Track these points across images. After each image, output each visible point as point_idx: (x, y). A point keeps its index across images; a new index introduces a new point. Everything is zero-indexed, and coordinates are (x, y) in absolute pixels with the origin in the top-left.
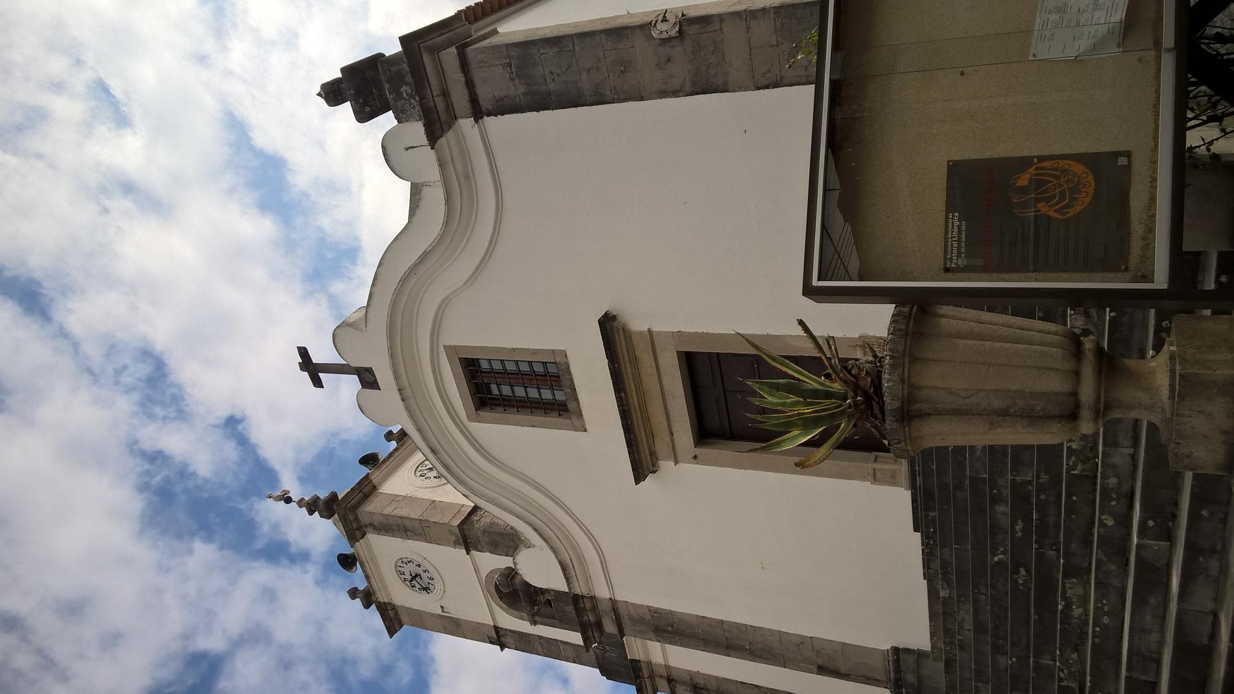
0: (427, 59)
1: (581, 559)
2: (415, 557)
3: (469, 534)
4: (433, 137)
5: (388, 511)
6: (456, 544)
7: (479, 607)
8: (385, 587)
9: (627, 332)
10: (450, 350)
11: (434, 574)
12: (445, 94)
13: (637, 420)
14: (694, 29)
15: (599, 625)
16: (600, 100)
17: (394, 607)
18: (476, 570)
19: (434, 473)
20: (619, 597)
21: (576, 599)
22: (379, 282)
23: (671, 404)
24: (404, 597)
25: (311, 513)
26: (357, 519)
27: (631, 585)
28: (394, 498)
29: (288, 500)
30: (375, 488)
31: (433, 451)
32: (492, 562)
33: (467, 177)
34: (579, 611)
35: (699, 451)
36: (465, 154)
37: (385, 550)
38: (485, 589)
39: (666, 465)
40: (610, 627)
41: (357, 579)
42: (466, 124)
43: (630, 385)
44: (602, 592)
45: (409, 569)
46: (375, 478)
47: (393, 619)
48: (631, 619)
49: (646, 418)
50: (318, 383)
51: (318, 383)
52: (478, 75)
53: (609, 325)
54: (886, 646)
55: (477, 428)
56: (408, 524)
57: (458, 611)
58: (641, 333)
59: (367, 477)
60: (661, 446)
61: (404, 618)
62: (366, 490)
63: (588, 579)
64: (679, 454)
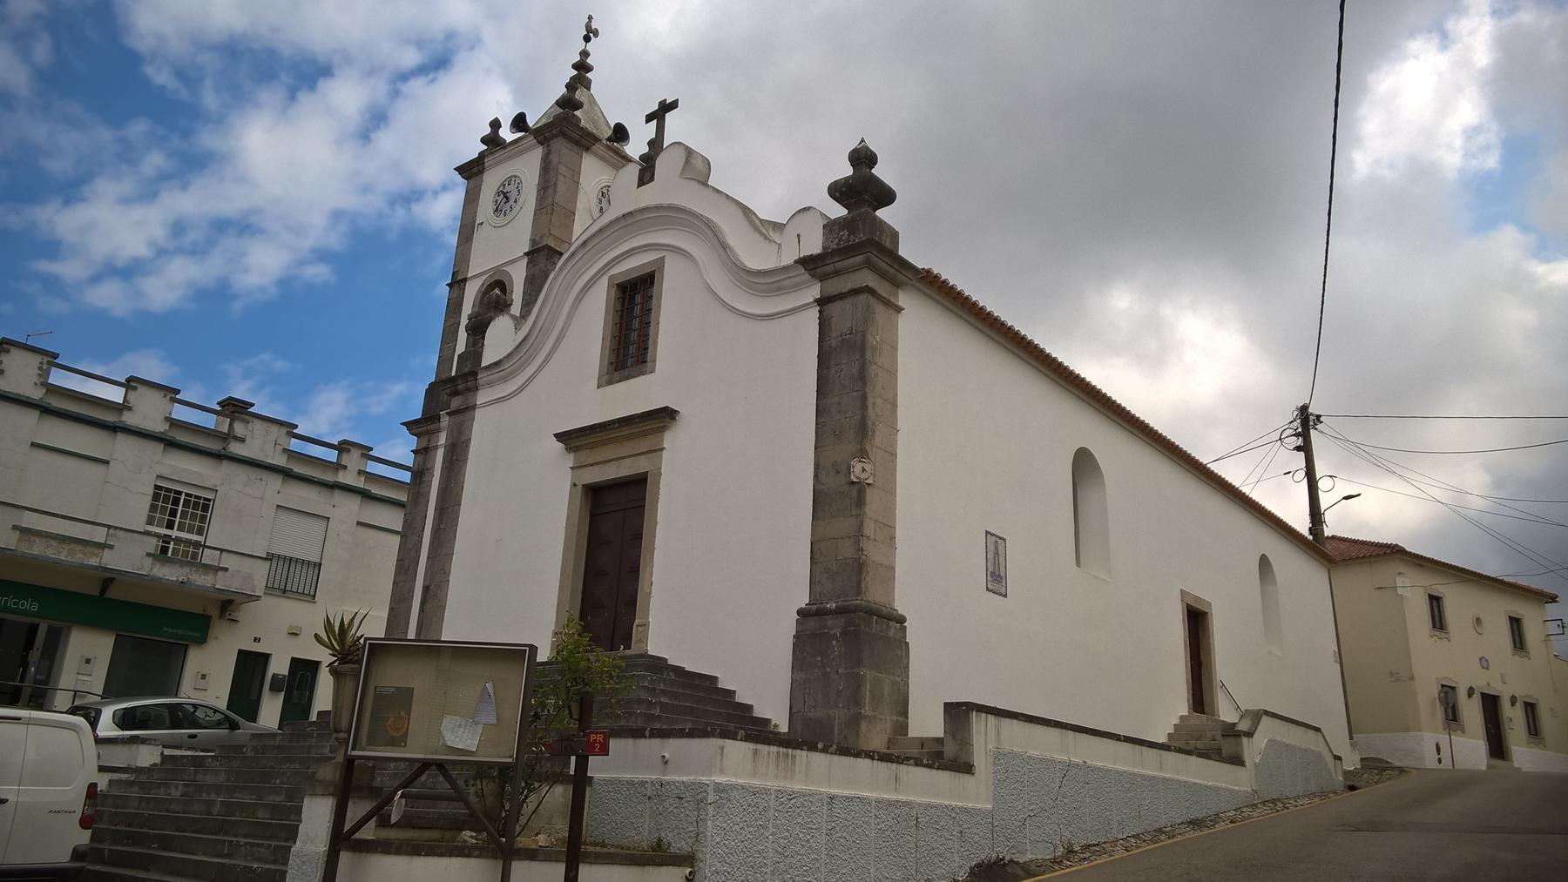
0: (860, 258)
1: (505, 379)
2: (523, 197)
3: (542, 256)
4: (807, 263)
5: (563, 170)
6: (533, 241)
7: (481, 264)
8: (497, 164)
9: (662, 429)
10: (661, 262)
11: (510, 216)
12: (837, 273)
13: (601, 436)
14: (854, 492)
15: (456, 393)
16: (819, 412)
17: (481, 172)
18: (512, 262)
19: (596, 213)
20: (478, 413)
21: (474, 374)
22: (715, 195)
23: (613, 465)
24: (491, 181)
25: (575, 66)
26: (554, 137)
27: (486, 426)
28: (576, 173)
29: (587, 39)
30: (587, 149)
31: (584, 243)
32: (518, 276)
33: (779, 289)
34: (465, 375)
35: (579, 487)
36: (796, 288)
37: (527, 167)
38: (498, 270)
39: (570, 460)
40: (456, 403)
41: (506, 134)
42: (815, 291)
43: (626, 431)
44: (482, 397)
45: (511, 188)
46: (597, 147)
47: (471, 171)
48: (462, 423)
49: (603, 443)
50: (649, 118)
51: (649, 118)
52: (847, 304)
53: (665, 416)
54: (900, 607)
55: (603, 283)
56: (550, 191)
57: (480, 237)
58: (662, 441)
59: (597, 140)
60: (584, 456)
61: (473, 181)
62: (585, 141)
63: (491, 384)
64: (579, 471)
